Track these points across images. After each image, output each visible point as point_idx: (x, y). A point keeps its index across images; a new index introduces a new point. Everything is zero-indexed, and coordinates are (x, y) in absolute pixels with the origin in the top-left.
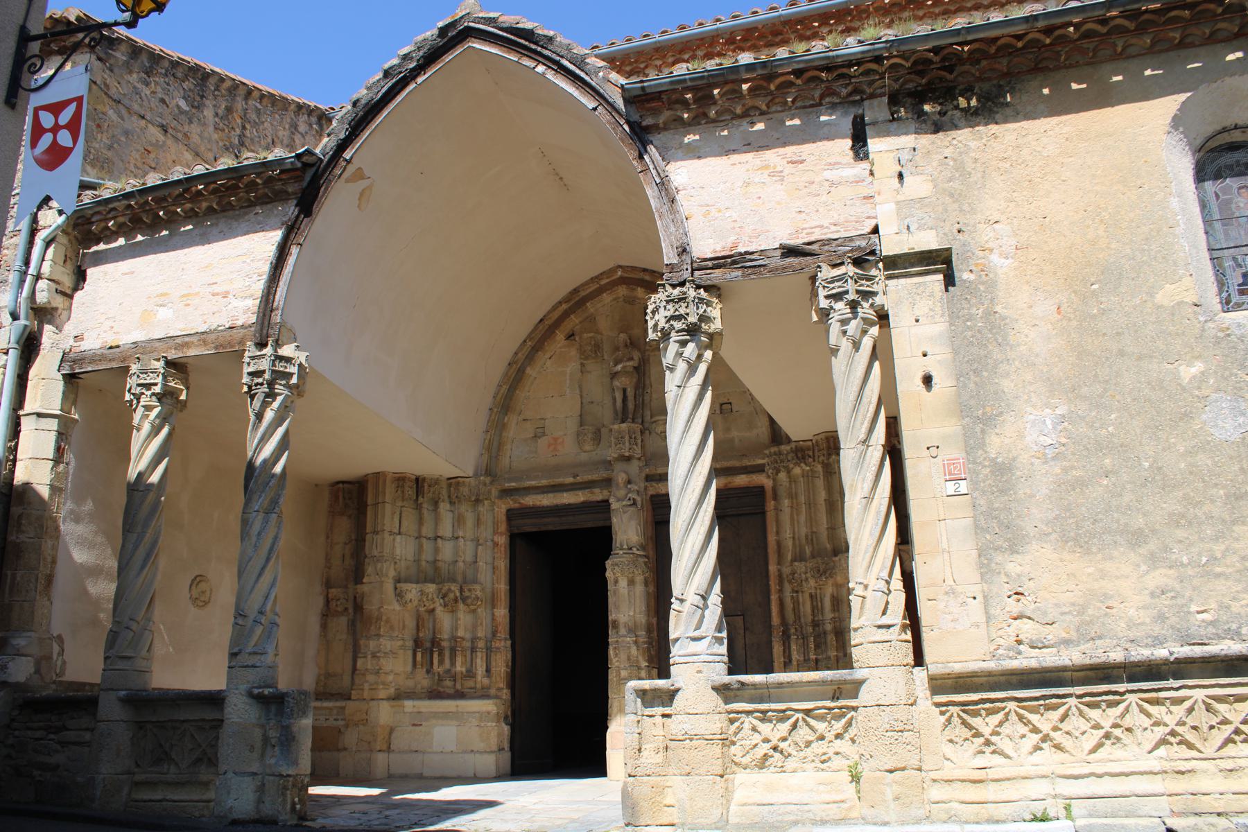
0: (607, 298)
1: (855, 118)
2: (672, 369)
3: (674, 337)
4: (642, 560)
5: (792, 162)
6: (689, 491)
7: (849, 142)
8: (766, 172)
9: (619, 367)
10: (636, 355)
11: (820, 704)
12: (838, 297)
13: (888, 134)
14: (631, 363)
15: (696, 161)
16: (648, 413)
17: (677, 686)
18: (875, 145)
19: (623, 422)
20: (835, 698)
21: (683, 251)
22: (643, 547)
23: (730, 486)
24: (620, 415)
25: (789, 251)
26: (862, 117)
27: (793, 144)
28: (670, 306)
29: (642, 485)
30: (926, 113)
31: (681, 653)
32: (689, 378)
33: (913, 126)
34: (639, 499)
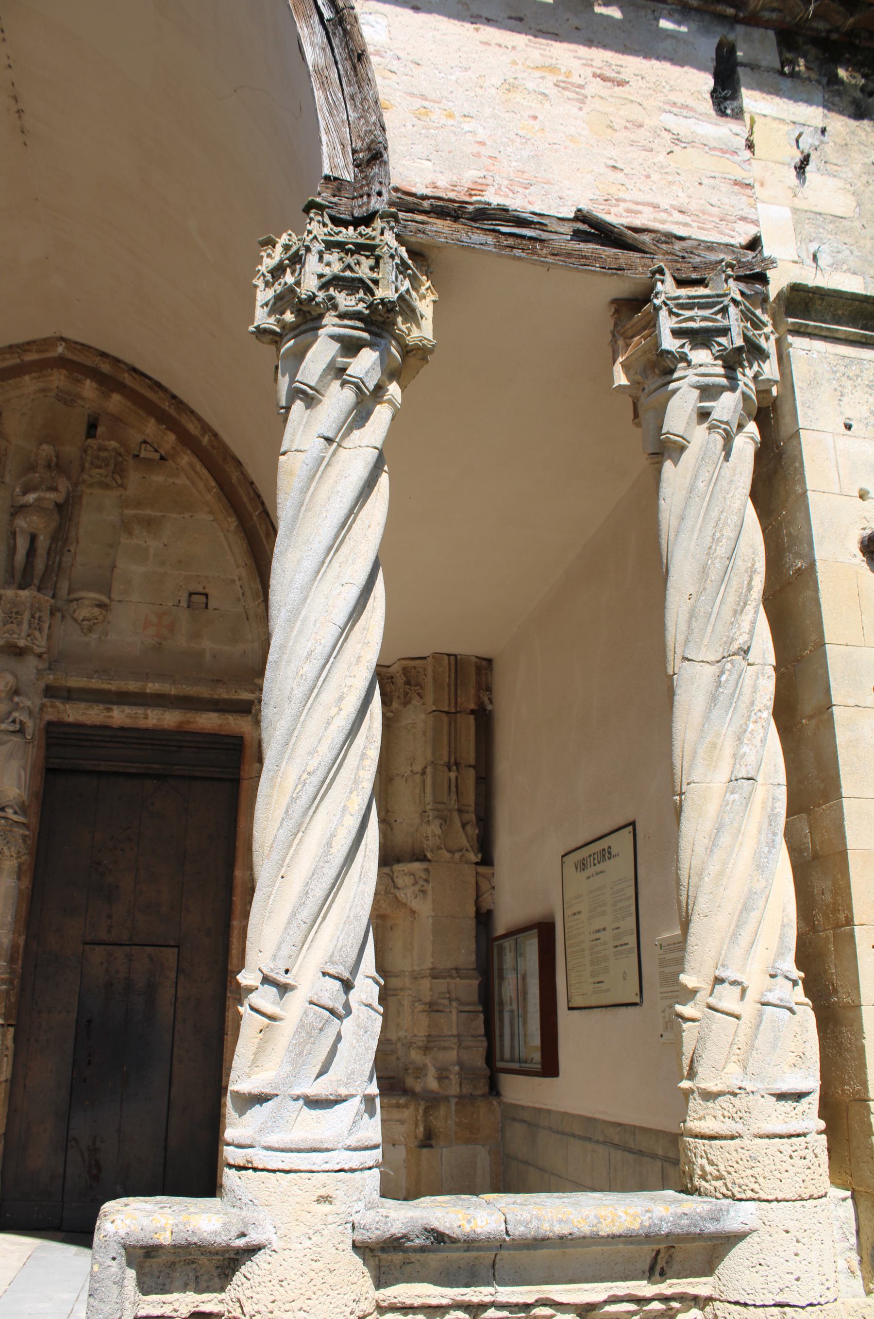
0: (29, 384)
1: (720, 47)
2: (311, 400)
3: (331, 324)
4: (19, 831)
5: (604, 79)
6: (328, 696)
7: (707, 81)
8: (551, 78)
9: (31, 497)
10: (64, 485)
11: (622, 1288)
12: (700, 338)
13: (776, 91)
14: (52, 495)
15: (408, 13)
16: (64, 585)
17: (254, 1237)
18: (751, 100)
19: (21, 587)
20: (656, 1270)
21: (372, 156)
22: (23, 809)
23: (187, 727)
24: (18, 576)
25: (594, 230)
26: (732, 49)
27: (605, 47)
28: (333, 257)
29: (38, 702)
30: (841, 82)
31: (274, 1139)
32: (350, 430)
33: (819, 95)
34: (30, 724)
